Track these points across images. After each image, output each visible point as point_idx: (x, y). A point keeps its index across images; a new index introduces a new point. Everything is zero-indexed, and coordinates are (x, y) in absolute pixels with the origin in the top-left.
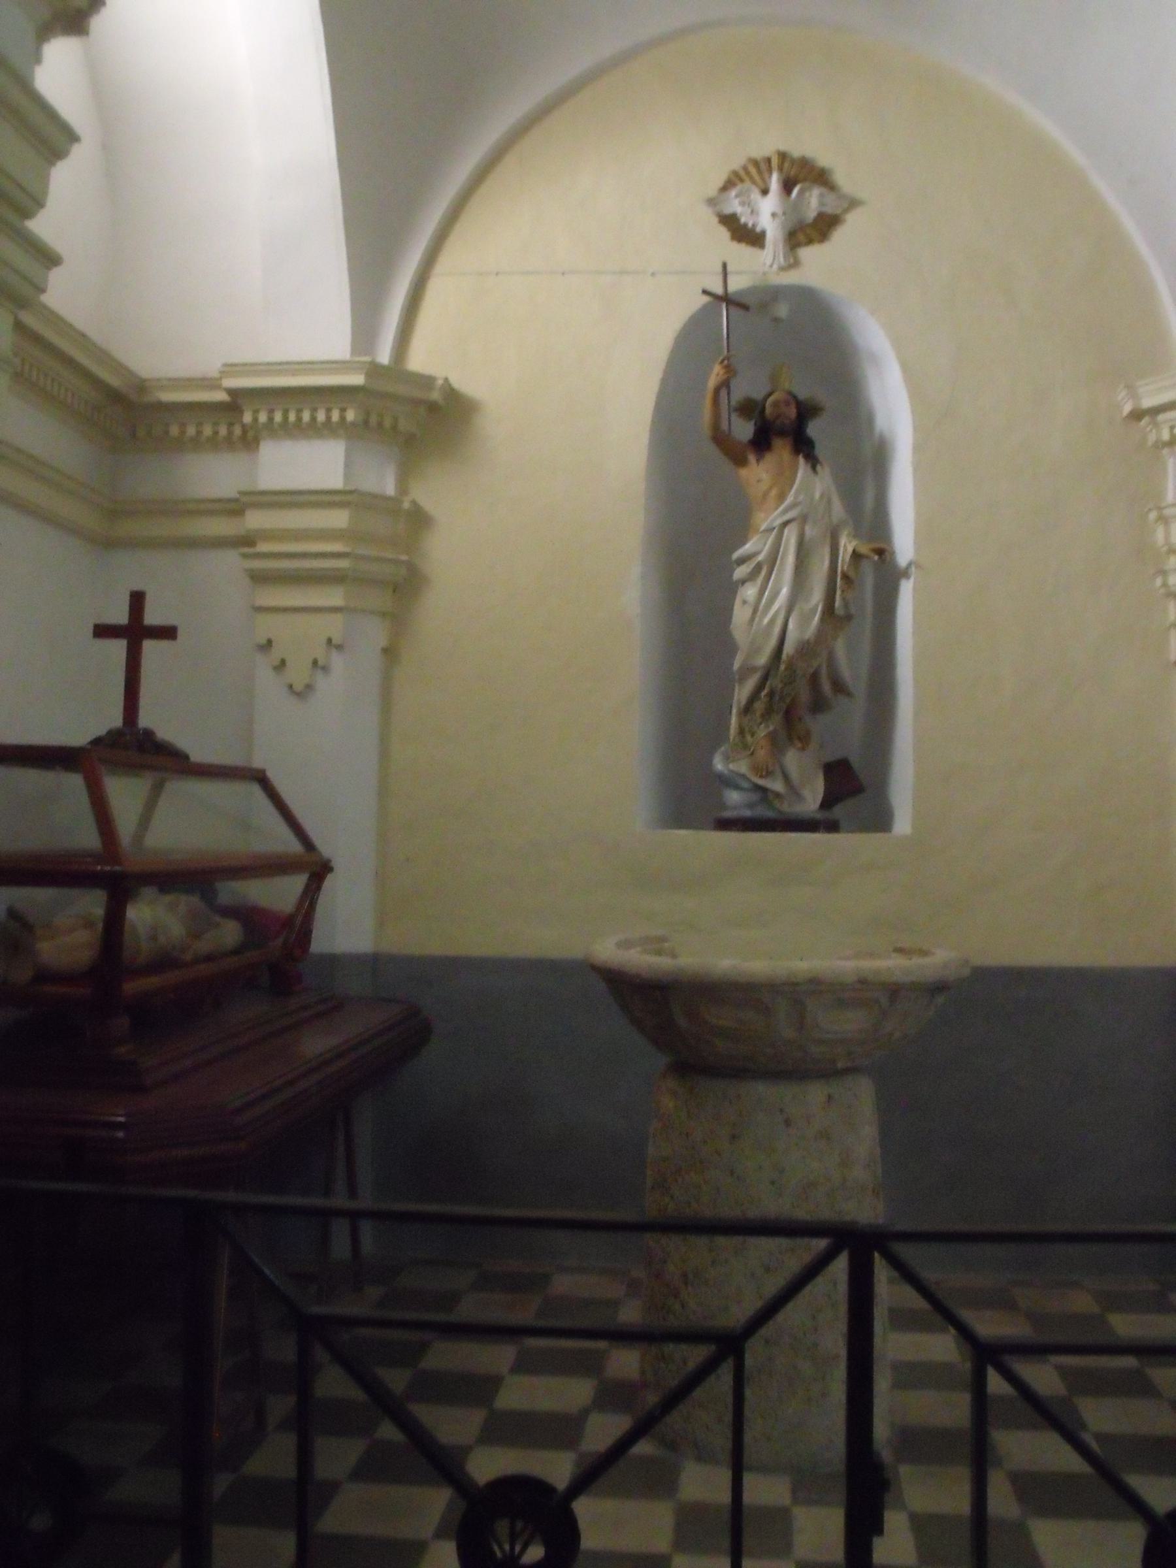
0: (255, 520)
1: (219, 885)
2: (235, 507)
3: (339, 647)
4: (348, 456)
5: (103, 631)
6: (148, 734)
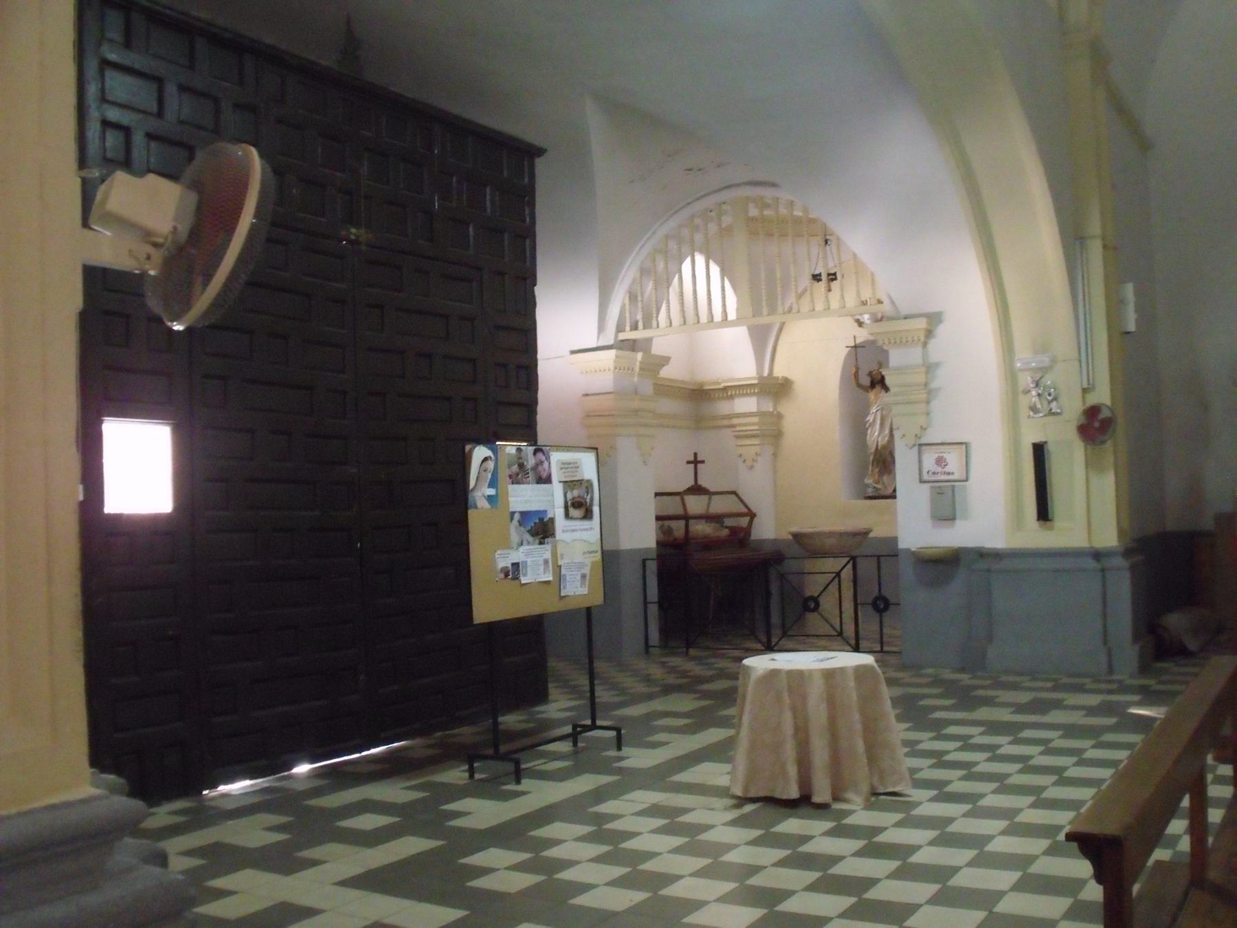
0: (735, 421)
1: (725, 520)
2: (730, 417)
3: (760, 455)
4: (758, 402)
5: (689, 462)
6: (700, 486)
